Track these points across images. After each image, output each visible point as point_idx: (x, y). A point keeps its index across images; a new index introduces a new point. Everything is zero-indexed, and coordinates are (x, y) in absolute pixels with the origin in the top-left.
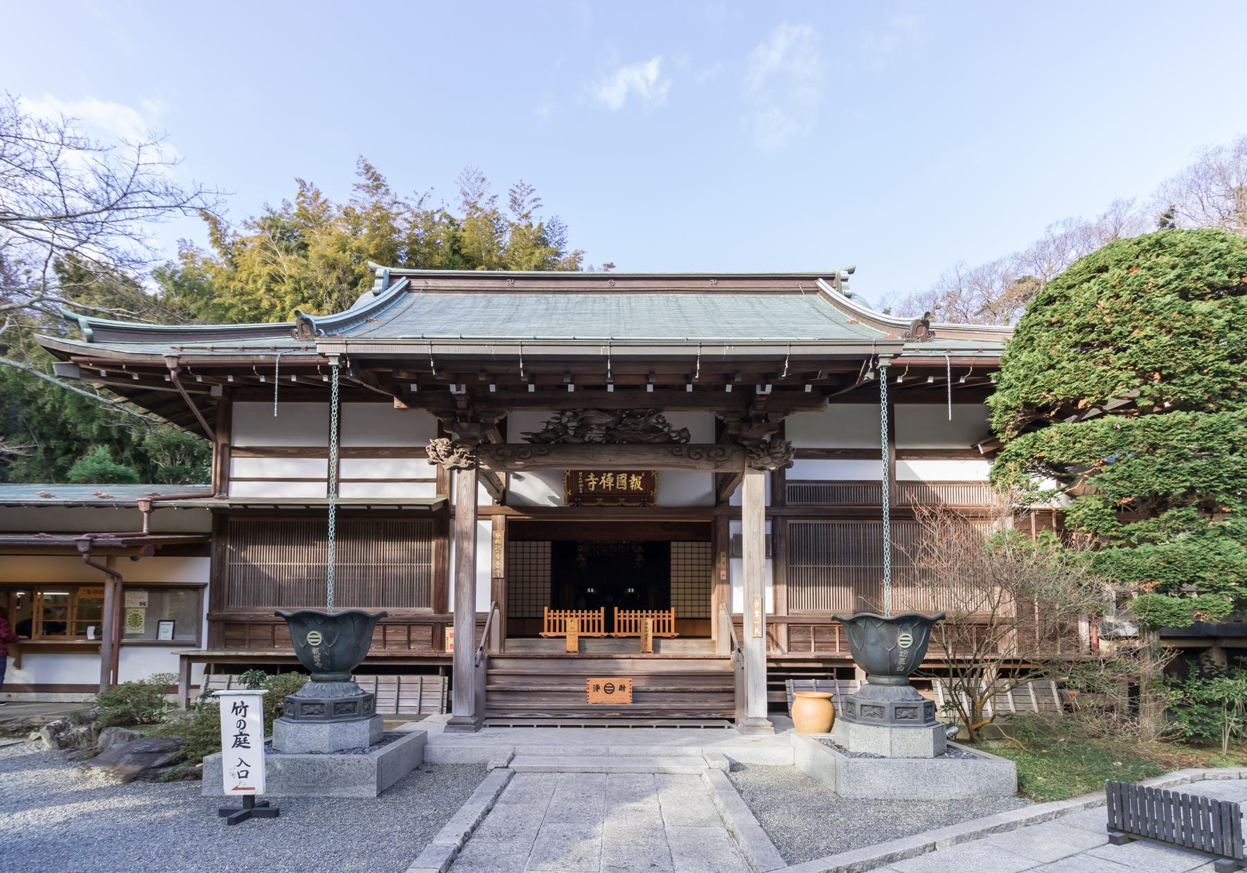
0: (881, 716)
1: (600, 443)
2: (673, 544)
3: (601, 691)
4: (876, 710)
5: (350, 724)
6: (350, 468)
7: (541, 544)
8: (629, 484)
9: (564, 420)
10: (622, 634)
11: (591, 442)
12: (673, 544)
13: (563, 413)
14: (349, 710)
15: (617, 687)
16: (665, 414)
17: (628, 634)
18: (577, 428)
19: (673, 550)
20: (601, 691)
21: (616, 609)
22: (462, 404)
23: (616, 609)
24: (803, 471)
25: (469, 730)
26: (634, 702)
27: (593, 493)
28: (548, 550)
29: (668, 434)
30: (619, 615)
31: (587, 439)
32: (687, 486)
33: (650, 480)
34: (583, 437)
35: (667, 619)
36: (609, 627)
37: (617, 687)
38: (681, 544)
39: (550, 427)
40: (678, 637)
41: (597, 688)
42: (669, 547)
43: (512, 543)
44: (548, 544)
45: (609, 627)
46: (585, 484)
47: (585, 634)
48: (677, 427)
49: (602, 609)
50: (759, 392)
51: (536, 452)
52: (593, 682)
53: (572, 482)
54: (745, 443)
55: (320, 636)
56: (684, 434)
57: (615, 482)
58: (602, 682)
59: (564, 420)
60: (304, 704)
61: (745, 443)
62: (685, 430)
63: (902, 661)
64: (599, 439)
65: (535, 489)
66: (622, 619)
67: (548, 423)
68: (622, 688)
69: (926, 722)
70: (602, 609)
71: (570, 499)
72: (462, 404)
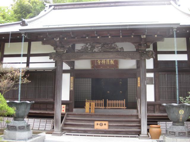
0: (175, 135)
1: (98, 52)
2: (128, 79)
3: (99, 125)
4: (173, 133)
5: (22, 132)
6: (32, 59)
7: (88, 79)
8: (110, 62)
9: (87, 46)
10: (109, 107)
11: (95, 52)
12: (128, 79)
13: (87, 44)
14: (22, 129)
15: (104, 124)
16: (116, 43)
17: (111, 107)
18: (91, 48)
19: (129, 81)
20: (99, 125)
21: (107, 100)
22: (58, 43)
23: (107, 100)
24: (161, 58)
25: (59, 135)
26: (109, 128)
27: (99, 65)
28: (91, 81)
29: (117, 49)
30: (108, 102)
31: (93, 51)
32: (128, 64)
33: (116, 63)
34: (93, 50)
35: (101, 103)
36: (105, 105)
37: (104, 124)
38: (131, 79)
39: (83, 48)
40: (126, 109)
41: (98, 124)
42: (127, 80)
43: (76, 79)
44: (91, 79)
45: (105, 105)
46: (97, 63)
47: (96, 107)
48: (120, 47)
49: (125, 100)
50: (142, 37)
51: (81, 55)
52: (96, 122)
53: (93, 63)
54: (140, 51)
55: (183, 111)
56: (122, 49)
57: (106, 62)
58: (99, 122)
59: (87, 46)
60: (11, 127)
61: (140, 51)
62: (122, 48)
63: (181, 118)
64: (97, 51)
65: (83, 64)
66: (109, 103)
67: (83, 47)
68: (105, 124)
69: (188, 137)
70: (125, 100)
71: (92, 67)
72: (58, 43)
